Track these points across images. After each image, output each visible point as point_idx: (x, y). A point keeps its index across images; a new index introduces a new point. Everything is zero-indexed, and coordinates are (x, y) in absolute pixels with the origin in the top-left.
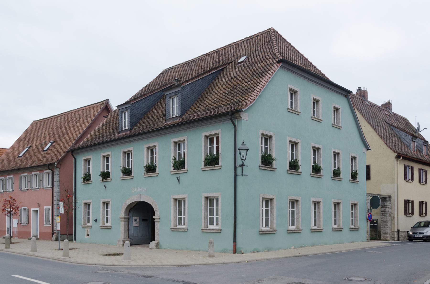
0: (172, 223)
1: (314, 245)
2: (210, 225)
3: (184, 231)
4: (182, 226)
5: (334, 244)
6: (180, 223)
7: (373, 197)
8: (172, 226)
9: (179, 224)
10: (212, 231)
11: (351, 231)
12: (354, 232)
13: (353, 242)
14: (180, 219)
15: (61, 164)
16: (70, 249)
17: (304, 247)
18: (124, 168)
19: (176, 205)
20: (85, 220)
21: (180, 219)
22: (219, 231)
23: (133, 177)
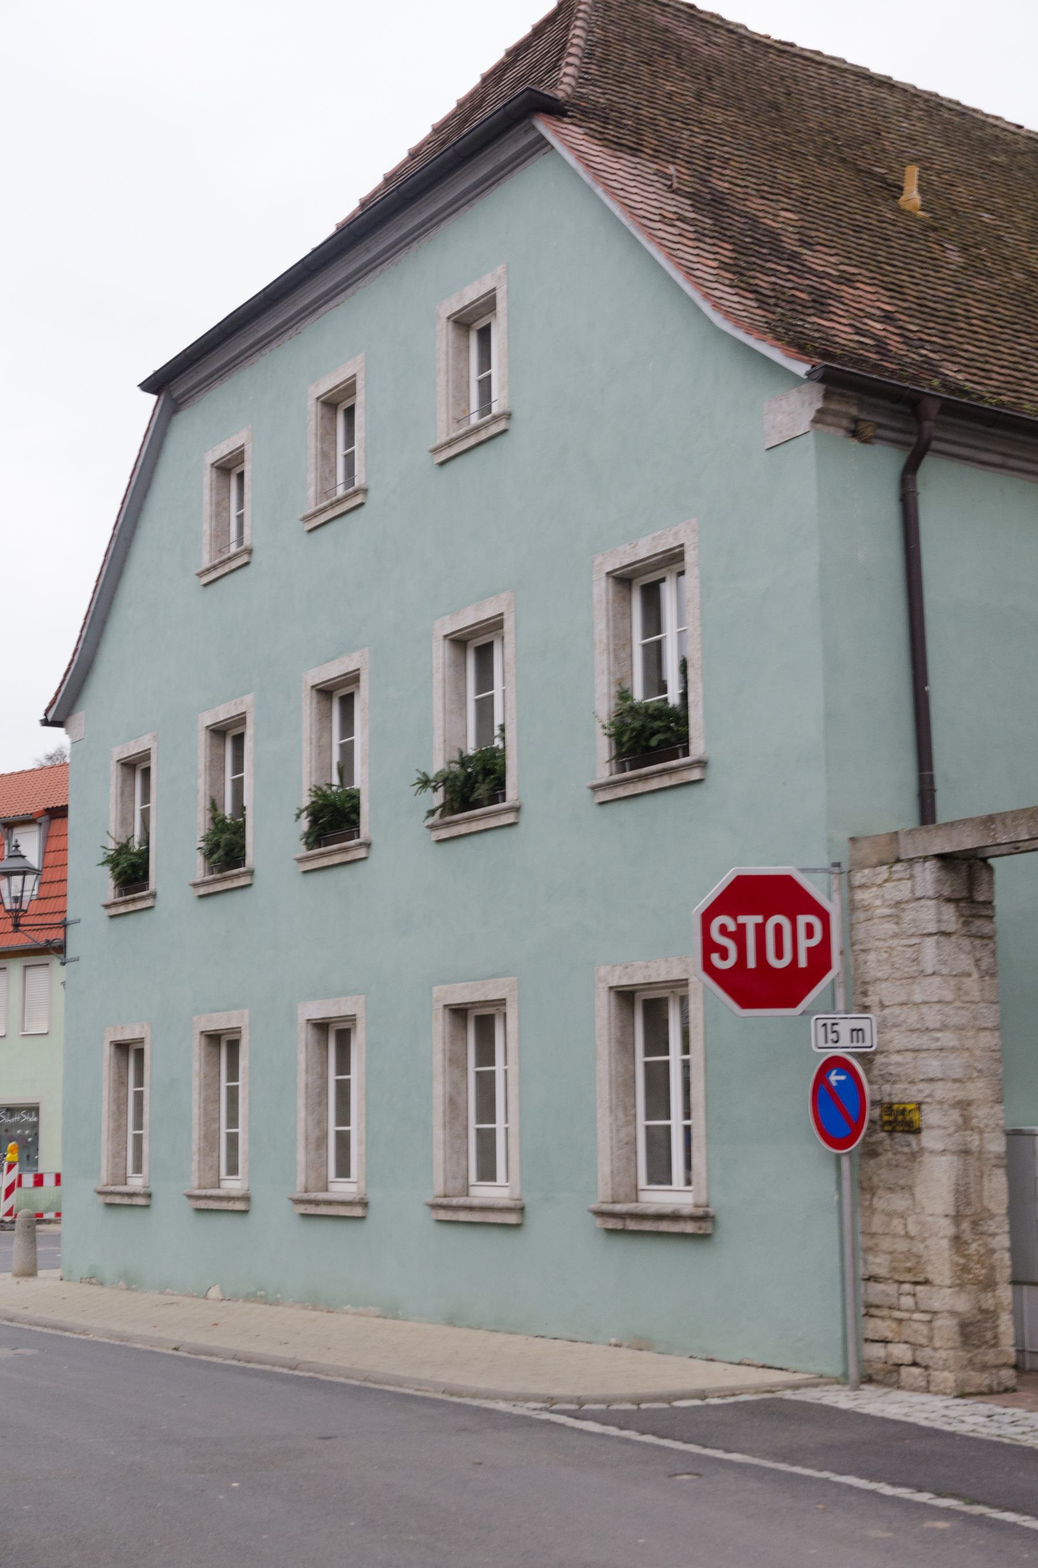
0: (604, 1168)
1: (314, 1302)
2: (671, 1183)
3: (698, 1228)
4: (674, 1197)
5: (451, 1321)
6: (660, 1174)
7: (445, 781)
8: (601, 1196)
9: (652, 1179)
10: (632, 1225)
11: (621, 1246)
12: (125, 1217)
13: (641, 1345)
14: (659, 1143)
15: (425, 782)
16: (866, 1340)
17: (265, 1301)
18: (318, 792)
19: (325, 1063)
20: (118, 1154)
21: (659, 1143)
22: (358, 1212)
23: (516, 809)
